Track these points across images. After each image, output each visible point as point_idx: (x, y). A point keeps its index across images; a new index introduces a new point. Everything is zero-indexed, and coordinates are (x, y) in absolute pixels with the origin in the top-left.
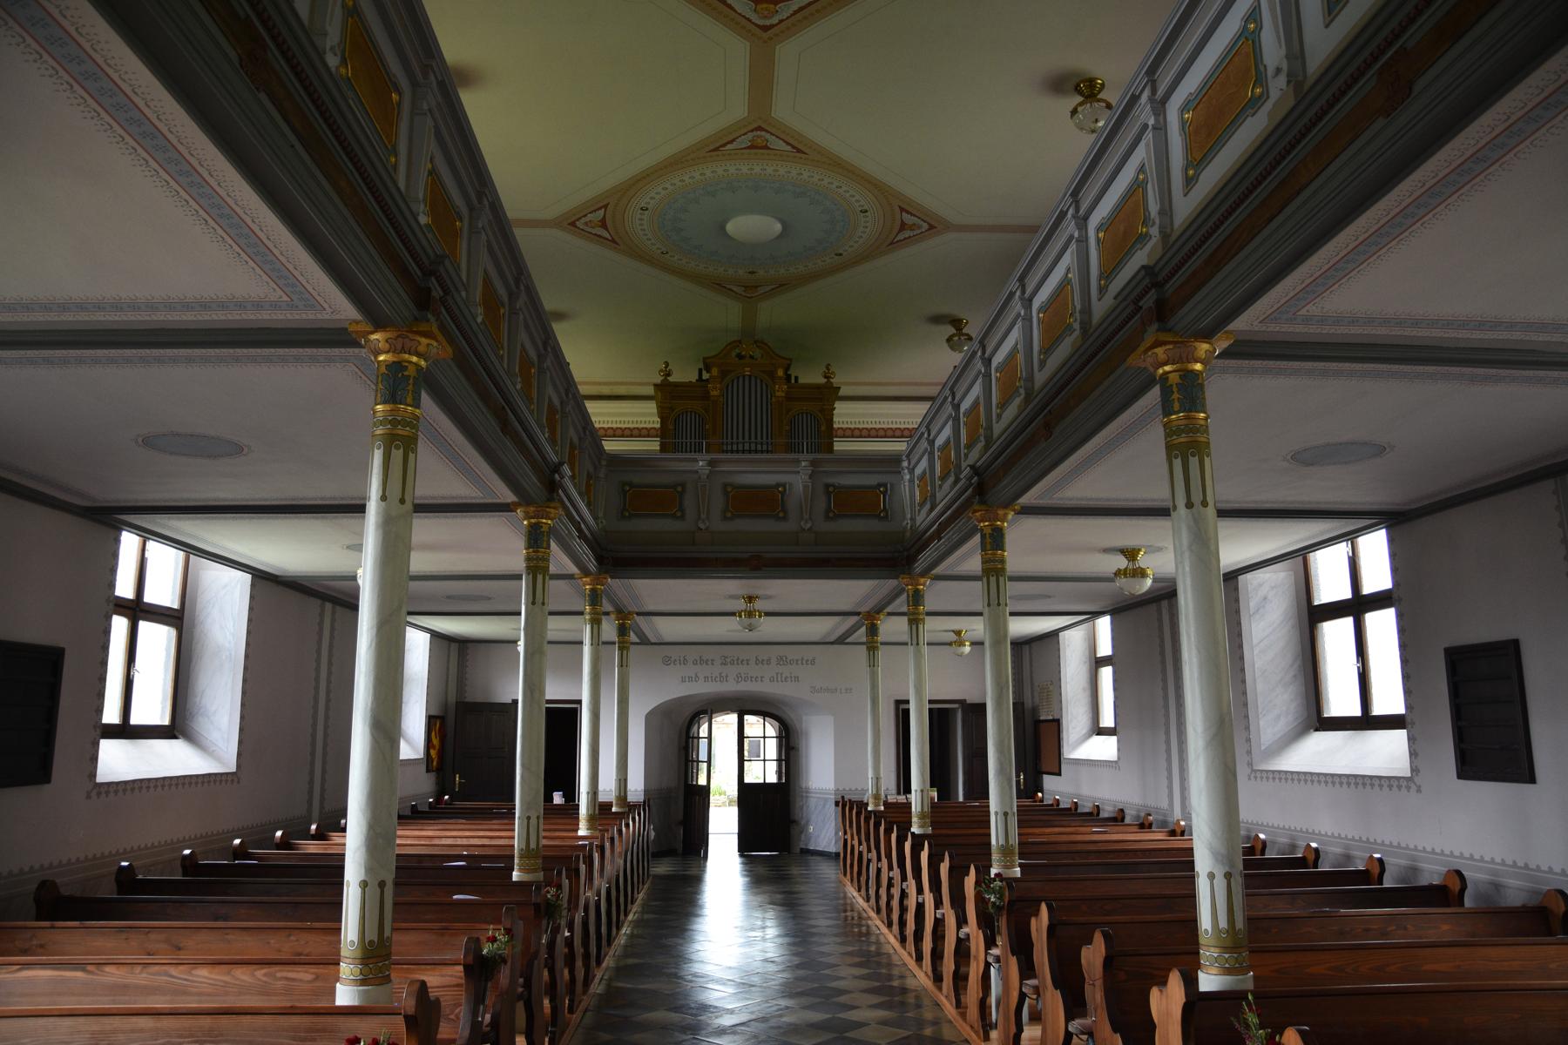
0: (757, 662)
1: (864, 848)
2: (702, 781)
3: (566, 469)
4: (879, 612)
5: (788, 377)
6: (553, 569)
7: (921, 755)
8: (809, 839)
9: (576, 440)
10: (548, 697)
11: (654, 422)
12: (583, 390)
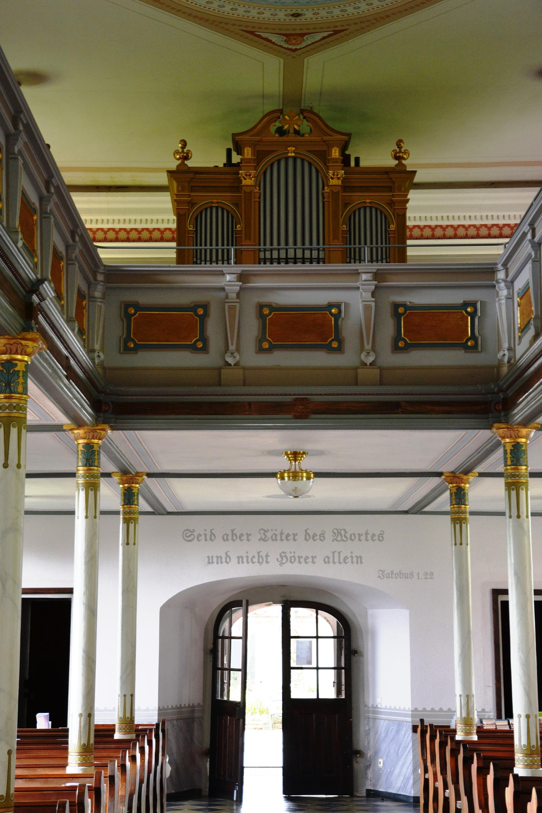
0: (308, 537)
1: (450, 793)
2: (235, 696)
3: (47, 288)
4: (467, 472)
5: (346, 159)
6: (31, 418)
7: (525, 665)
8: (377, 777)
9: (61, 248)
10: (26, 584)
11: (168, 220)
12: (69, 178)
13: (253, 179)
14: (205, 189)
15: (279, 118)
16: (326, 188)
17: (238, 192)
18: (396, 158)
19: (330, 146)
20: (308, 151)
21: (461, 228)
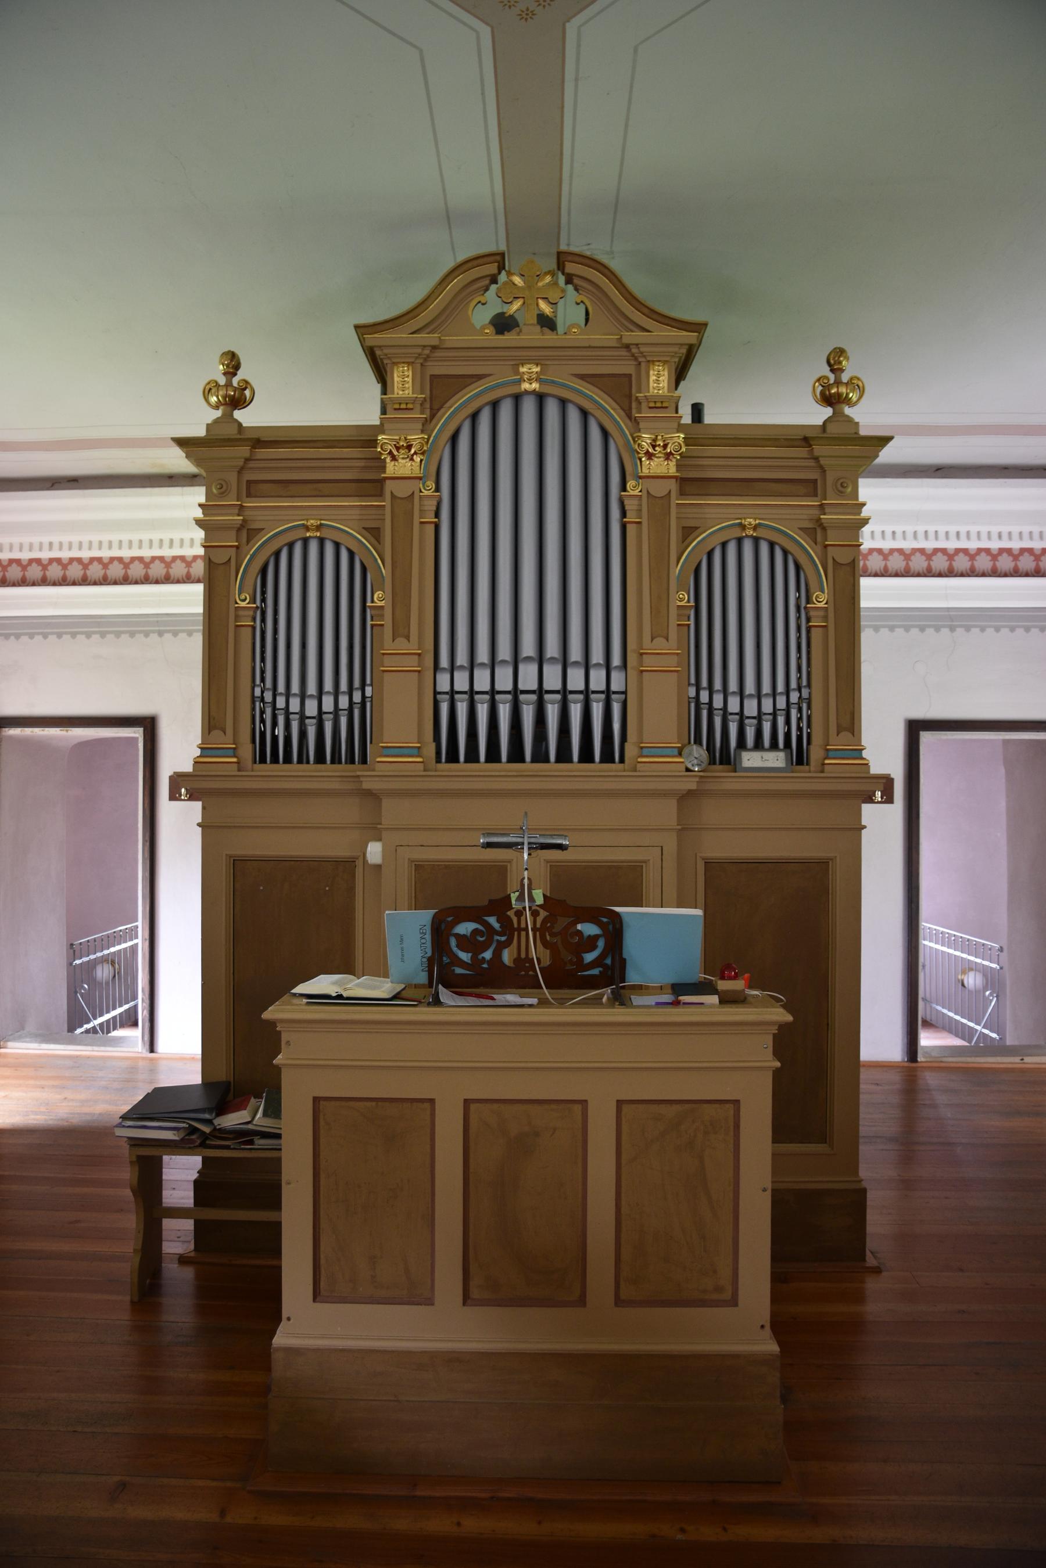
13: (417, 459)
14: (286, 487)
15: (494, 280)
16: (630, 484)
17: (380, 495)
18: (828, 399)
19: (641, 361)
20: (582, 377)
21: (875, 554)
